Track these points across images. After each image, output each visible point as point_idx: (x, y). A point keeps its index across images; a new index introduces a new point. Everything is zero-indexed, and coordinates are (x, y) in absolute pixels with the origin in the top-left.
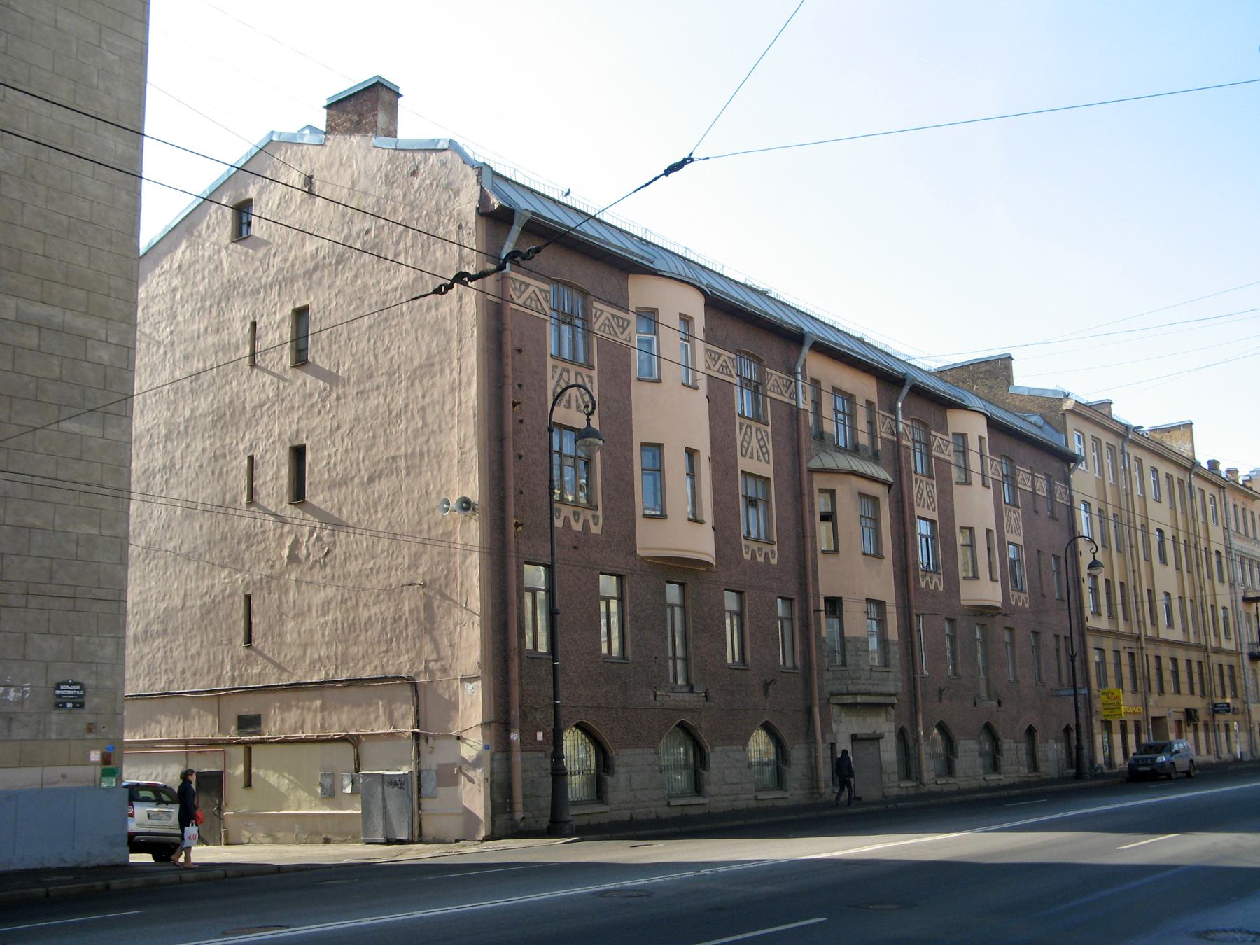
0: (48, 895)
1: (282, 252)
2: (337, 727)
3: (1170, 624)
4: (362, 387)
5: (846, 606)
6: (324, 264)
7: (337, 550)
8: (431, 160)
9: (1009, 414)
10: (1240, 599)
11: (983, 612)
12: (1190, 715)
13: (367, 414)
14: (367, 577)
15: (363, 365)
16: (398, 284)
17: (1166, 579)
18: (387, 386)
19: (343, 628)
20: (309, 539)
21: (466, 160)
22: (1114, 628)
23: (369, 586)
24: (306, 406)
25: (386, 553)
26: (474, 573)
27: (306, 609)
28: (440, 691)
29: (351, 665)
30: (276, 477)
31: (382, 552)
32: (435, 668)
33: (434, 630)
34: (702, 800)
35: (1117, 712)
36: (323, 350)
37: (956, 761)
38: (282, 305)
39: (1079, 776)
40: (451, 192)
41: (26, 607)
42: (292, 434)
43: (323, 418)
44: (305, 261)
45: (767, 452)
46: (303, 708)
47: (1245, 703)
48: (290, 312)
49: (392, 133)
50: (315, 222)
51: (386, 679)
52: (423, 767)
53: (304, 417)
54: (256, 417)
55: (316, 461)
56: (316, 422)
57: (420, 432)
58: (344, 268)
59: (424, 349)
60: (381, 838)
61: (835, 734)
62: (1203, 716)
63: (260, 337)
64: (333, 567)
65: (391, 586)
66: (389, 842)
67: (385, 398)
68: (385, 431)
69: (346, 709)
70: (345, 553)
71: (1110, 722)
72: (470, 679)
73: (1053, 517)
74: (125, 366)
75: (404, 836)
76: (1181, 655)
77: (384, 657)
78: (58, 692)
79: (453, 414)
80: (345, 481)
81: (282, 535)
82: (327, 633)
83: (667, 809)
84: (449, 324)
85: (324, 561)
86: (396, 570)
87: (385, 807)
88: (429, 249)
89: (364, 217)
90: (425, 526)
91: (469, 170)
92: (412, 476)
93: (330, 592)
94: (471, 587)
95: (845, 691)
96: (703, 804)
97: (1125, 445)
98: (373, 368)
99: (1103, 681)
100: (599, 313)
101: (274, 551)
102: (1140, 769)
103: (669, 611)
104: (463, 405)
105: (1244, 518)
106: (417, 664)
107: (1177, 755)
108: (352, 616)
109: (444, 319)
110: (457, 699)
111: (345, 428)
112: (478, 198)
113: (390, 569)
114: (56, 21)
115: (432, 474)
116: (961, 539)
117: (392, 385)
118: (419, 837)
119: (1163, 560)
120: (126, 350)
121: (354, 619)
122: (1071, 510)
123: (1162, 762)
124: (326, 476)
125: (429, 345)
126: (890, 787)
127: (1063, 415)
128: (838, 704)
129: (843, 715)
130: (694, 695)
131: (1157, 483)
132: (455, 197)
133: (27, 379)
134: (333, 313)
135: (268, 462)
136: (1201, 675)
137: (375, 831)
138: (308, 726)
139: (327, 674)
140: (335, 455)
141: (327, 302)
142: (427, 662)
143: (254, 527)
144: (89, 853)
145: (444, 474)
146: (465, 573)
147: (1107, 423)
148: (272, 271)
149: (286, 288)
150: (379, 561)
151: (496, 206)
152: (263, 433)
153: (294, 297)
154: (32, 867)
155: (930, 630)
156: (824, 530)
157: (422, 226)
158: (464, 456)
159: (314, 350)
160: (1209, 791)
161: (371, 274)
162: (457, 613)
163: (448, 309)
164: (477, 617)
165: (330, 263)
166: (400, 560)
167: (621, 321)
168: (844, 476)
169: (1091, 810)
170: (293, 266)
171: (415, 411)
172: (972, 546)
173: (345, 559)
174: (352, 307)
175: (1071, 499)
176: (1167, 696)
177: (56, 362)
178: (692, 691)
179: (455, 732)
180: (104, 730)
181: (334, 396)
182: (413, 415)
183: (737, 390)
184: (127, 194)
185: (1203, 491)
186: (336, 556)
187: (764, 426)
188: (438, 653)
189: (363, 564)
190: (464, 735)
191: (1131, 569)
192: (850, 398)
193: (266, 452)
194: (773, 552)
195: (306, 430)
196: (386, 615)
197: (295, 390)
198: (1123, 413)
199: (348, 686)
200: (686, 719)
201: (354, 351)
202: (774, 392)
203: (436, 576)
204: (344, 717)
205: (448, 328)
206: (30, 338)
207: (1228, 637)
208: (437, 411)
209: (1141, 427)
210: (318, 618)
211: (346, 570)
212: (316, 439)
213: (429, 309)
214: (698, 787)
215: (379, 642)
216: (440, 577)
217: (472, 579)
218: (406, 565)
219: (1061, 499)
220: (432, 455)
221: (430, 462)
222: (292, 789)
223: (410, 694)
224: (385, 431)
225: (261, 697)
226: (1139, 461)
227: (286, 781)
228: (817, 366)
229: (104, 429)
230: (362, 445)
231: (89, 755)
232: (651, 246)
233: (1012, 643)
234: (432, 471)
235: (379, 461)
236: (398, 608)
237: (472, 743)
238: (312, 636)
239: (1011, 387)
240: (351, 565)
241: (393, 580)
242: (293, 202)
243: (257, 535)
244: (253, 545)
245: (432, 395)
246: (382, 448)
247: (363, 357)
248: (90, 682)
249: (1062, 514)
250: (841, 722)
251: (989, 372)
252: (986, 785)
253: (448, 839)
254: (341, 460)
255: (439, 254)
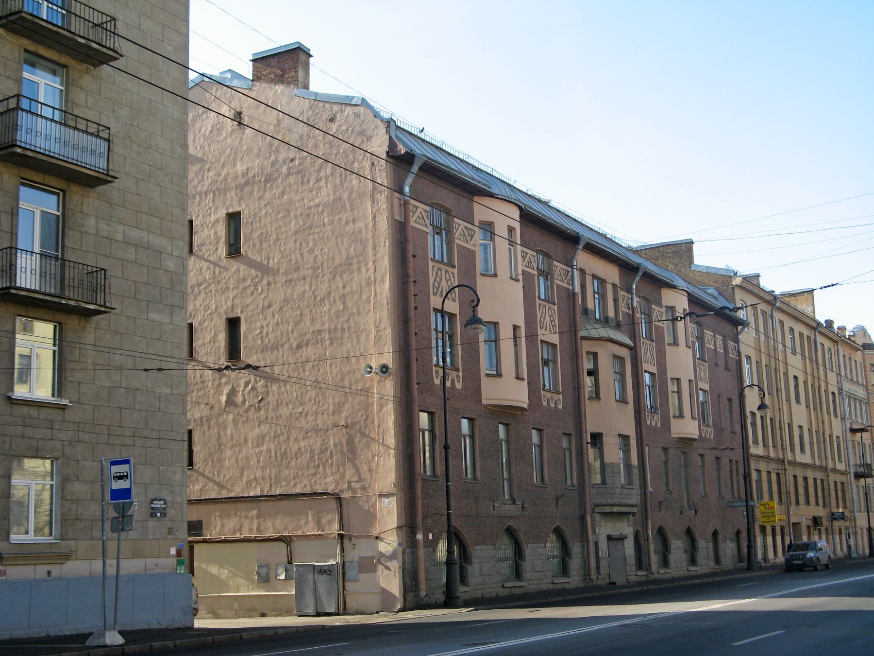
0: (175, 647)
1: (215, 168)
2: (271, 530)
3: (802, 450)
4: (290, 277)
5: (605, 439)
6: (254, 181)
7: (270, 398)
8: (347, 111)
9: (701, 291)
10: (848, 430)
11: (686, 442)
12: (816, 521)
13: (295, 297)
14: (297, 419)
15: (290, 260)
16: (320, 202)
17: (800, 415)
18: (312, 278)
19: (276, 456)
20: (245, 388)
21: (376, 115)
22: (766, 454)
23: (298, 425)
24: (240, 288)
25: (313, 402)
26: (389, 419)
27: (242, 441)
28: (361, 503)
29: (284, 483)
30: (214, 340)
31: (310, 400)
32: (356, 487)
33: (356, 459)
34: (522, 584)
35: (772, 519)
36: (254, 246)
37: (670, 556)
38: (216, 209)
39: (750, 568)
40: (364, 138)
41: (134, 446)
42: (228, 308)
43: (256, 298)
44: (237, 177)
45: (555, 325)
46: (241, 517)
47: (851, 512)
48: (224, 215)
49: (306, 87)
50: (245, 148)
51: (315, 494)
52: (346, 559)
53: (238, 296)
54: (194, 294)
55: (250, 330)
56: (249, 300)
57: (341, 313)
58: (272, 185)
59: (344, 252)
60: (313, 612)
61: (598, 535)
62: (825, 522)
63: (197, 232)
64: (267, 410)
65: (318, 426)
66: (318, 615)
67: (311, 287)
68: (311, 311)
69: (279, 517)
70: (277, 400)
71: (765, 526)
72: (387, 495)
73: (727, 369)
74: (181, 272)
75: (332, 609)
76: (810, 474)
77: (312, 478)
78: (152, 506)
79: (369, 302)
80: (275, 347)
81: (220, 384)
82: (262, 460)
83: (502, 589)
84: (364, 235)
85: (258, 406)
86: (322, 415)
87: (315, 589)
88: (346, 178)
89: (289, 149)
90: (347, 383)
91: (380, 123)
92: (335, 345)
93: (264, 428)
94: (387, 429)
95: (605, 503)
96: (523, 586)
97: (773, 310)
98: (300, 263)
99: (760, 497)
100: (457, 226)
101: (213, 397)
102: (794, 562)
103: (421, 433)
104: (378, 296)
105: (851, 365)
106: (340, 484)
107: (820, 552)
108: (284, 447)
109: (360, 231)
110: (375, 510)
111: (276, 307)
112: (388, 144)
113: (316, 413)
114: (140, 24)
115: (352, 345)
116: (672, 387)
117: (317, 277)
118: (344, 611)
119: (798, 401)
120: (183, 260)
121: (286, 449)
122: (739, 363)
123: (811, 558)
124: (259, 342)
125: (347, 250)
126: (630, 575)
127: (733, 288)
128: (599, 513)
129: (602, 521)
130: (516, 506)
131: (793, 339)
132: (367, 142)
133: (130, 283)
134: (262, 219)
135: (206, 328)
136: (823, 490)
137: (307, 607)
138: (246, 529)
139: (262, 490)
140: (267, 326)
141: (257, 210)
142: (349, 483)
143: (194, 377)
144: (173, 619)
145: (362, 345)
146: (381, 418)
147: (756, 291)
148: (207, 183)
149: (219, 197)
150: (307, 408)
151: (403, 152)
152: (201, 306)
153: (227, 204)
154: (144, 628)
155: (653, 456)
156: (588, 381)
157: (340, 160)
158: (379, 333)
159: (246, 246)
160: (863, 577)
161: (297, 192)
162: (374, 447)
163: (363, 224)
164: (392, 451)
165: (260, 181)
166: (325, 407)
167: (470, 231)
168: (603, 342)
169: (814, 586)
170: (226, 180)
171: (337, 298)
172: (679, 392)
173: (277, 405)
174: (280, 216)
175: (739, 354)
176: (811, 507)
177: (145, 270)
178: (514, 503)
179: (375, 533)
180: (177, 532)
181: (265, 282)
182: (335, 301)
183: (430, 238)
184: (180, 147)
185: (823, 345)
186: (269, 403)
187: (452, 269)
188: (359, 475)
189: (293, 409)
190: (382, 536)
191: (778, 408)
192: (602, 282)
193: (204, 321)
194: (559, 399)
195: (240, 306)
196: (314, 447)
197: (230, 275)
198: (766, 283)
199: (281, 500)
200: (511, 523)
201: (282, 249)
202: (460, 239)
203: (356, 419)
204: (278, 523)
205: (364, 238)
206: (131, 254)
207: (840, 461)
208: (356, 299)
209: (773, 292)
210: (253, 448)
211: (278, 413)
212: (250, 314)
213: (347, 223)
214: (518, 573)
215: (308, 467)
216: (360, 421)
217: (387, 422)
218: (331, 411)
219: (733, 355)
220: (352, 331)
221: (350, 336)
222: (231, 577)
223: (335, 506)
224: (311, 311)
225: (203, 508)
226: (781, 323)
227: (226, 571)
228: (583, 259)
229: (172, 318)
230: (291, 320)
231: (170, 550)
232: (483, 173)
233: (703, 466)
234: (352, 342)
235: (306, 333)
236: (324, 443)
237: (388, 542)
238: (248, 462)
239: (692, 265)
240: (282, 409)
241: (320, 421)
242: (224, 130)
243: (196, 384)
244: (193, 392)
245: (351, 287)
246: (308, 323)
247: (291, 255)
248: (169, 498)
249: (733, 366)
250: (601, 526)
251: (676, 253)
252: (688, 574)
253: (368, 612)
254: (273, 331)
255: (354, 182)
